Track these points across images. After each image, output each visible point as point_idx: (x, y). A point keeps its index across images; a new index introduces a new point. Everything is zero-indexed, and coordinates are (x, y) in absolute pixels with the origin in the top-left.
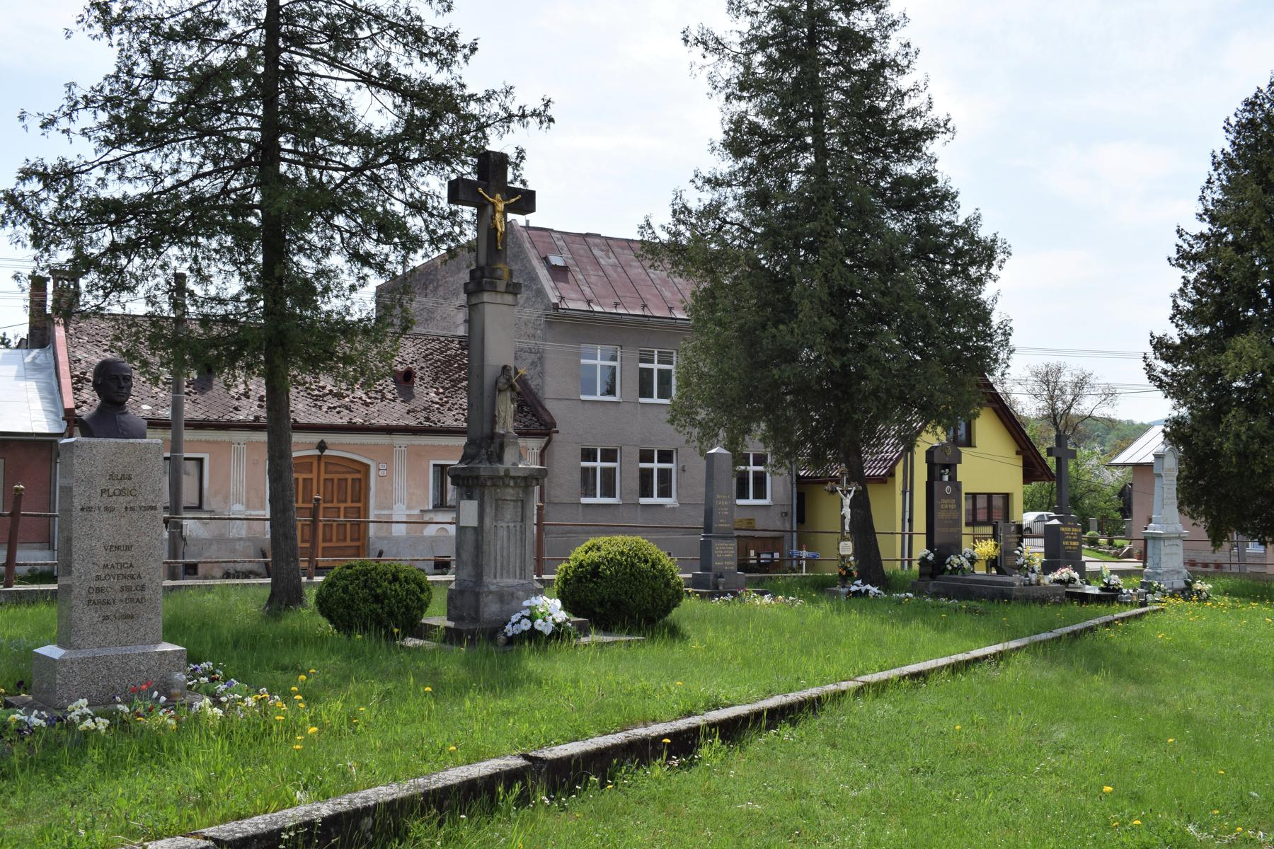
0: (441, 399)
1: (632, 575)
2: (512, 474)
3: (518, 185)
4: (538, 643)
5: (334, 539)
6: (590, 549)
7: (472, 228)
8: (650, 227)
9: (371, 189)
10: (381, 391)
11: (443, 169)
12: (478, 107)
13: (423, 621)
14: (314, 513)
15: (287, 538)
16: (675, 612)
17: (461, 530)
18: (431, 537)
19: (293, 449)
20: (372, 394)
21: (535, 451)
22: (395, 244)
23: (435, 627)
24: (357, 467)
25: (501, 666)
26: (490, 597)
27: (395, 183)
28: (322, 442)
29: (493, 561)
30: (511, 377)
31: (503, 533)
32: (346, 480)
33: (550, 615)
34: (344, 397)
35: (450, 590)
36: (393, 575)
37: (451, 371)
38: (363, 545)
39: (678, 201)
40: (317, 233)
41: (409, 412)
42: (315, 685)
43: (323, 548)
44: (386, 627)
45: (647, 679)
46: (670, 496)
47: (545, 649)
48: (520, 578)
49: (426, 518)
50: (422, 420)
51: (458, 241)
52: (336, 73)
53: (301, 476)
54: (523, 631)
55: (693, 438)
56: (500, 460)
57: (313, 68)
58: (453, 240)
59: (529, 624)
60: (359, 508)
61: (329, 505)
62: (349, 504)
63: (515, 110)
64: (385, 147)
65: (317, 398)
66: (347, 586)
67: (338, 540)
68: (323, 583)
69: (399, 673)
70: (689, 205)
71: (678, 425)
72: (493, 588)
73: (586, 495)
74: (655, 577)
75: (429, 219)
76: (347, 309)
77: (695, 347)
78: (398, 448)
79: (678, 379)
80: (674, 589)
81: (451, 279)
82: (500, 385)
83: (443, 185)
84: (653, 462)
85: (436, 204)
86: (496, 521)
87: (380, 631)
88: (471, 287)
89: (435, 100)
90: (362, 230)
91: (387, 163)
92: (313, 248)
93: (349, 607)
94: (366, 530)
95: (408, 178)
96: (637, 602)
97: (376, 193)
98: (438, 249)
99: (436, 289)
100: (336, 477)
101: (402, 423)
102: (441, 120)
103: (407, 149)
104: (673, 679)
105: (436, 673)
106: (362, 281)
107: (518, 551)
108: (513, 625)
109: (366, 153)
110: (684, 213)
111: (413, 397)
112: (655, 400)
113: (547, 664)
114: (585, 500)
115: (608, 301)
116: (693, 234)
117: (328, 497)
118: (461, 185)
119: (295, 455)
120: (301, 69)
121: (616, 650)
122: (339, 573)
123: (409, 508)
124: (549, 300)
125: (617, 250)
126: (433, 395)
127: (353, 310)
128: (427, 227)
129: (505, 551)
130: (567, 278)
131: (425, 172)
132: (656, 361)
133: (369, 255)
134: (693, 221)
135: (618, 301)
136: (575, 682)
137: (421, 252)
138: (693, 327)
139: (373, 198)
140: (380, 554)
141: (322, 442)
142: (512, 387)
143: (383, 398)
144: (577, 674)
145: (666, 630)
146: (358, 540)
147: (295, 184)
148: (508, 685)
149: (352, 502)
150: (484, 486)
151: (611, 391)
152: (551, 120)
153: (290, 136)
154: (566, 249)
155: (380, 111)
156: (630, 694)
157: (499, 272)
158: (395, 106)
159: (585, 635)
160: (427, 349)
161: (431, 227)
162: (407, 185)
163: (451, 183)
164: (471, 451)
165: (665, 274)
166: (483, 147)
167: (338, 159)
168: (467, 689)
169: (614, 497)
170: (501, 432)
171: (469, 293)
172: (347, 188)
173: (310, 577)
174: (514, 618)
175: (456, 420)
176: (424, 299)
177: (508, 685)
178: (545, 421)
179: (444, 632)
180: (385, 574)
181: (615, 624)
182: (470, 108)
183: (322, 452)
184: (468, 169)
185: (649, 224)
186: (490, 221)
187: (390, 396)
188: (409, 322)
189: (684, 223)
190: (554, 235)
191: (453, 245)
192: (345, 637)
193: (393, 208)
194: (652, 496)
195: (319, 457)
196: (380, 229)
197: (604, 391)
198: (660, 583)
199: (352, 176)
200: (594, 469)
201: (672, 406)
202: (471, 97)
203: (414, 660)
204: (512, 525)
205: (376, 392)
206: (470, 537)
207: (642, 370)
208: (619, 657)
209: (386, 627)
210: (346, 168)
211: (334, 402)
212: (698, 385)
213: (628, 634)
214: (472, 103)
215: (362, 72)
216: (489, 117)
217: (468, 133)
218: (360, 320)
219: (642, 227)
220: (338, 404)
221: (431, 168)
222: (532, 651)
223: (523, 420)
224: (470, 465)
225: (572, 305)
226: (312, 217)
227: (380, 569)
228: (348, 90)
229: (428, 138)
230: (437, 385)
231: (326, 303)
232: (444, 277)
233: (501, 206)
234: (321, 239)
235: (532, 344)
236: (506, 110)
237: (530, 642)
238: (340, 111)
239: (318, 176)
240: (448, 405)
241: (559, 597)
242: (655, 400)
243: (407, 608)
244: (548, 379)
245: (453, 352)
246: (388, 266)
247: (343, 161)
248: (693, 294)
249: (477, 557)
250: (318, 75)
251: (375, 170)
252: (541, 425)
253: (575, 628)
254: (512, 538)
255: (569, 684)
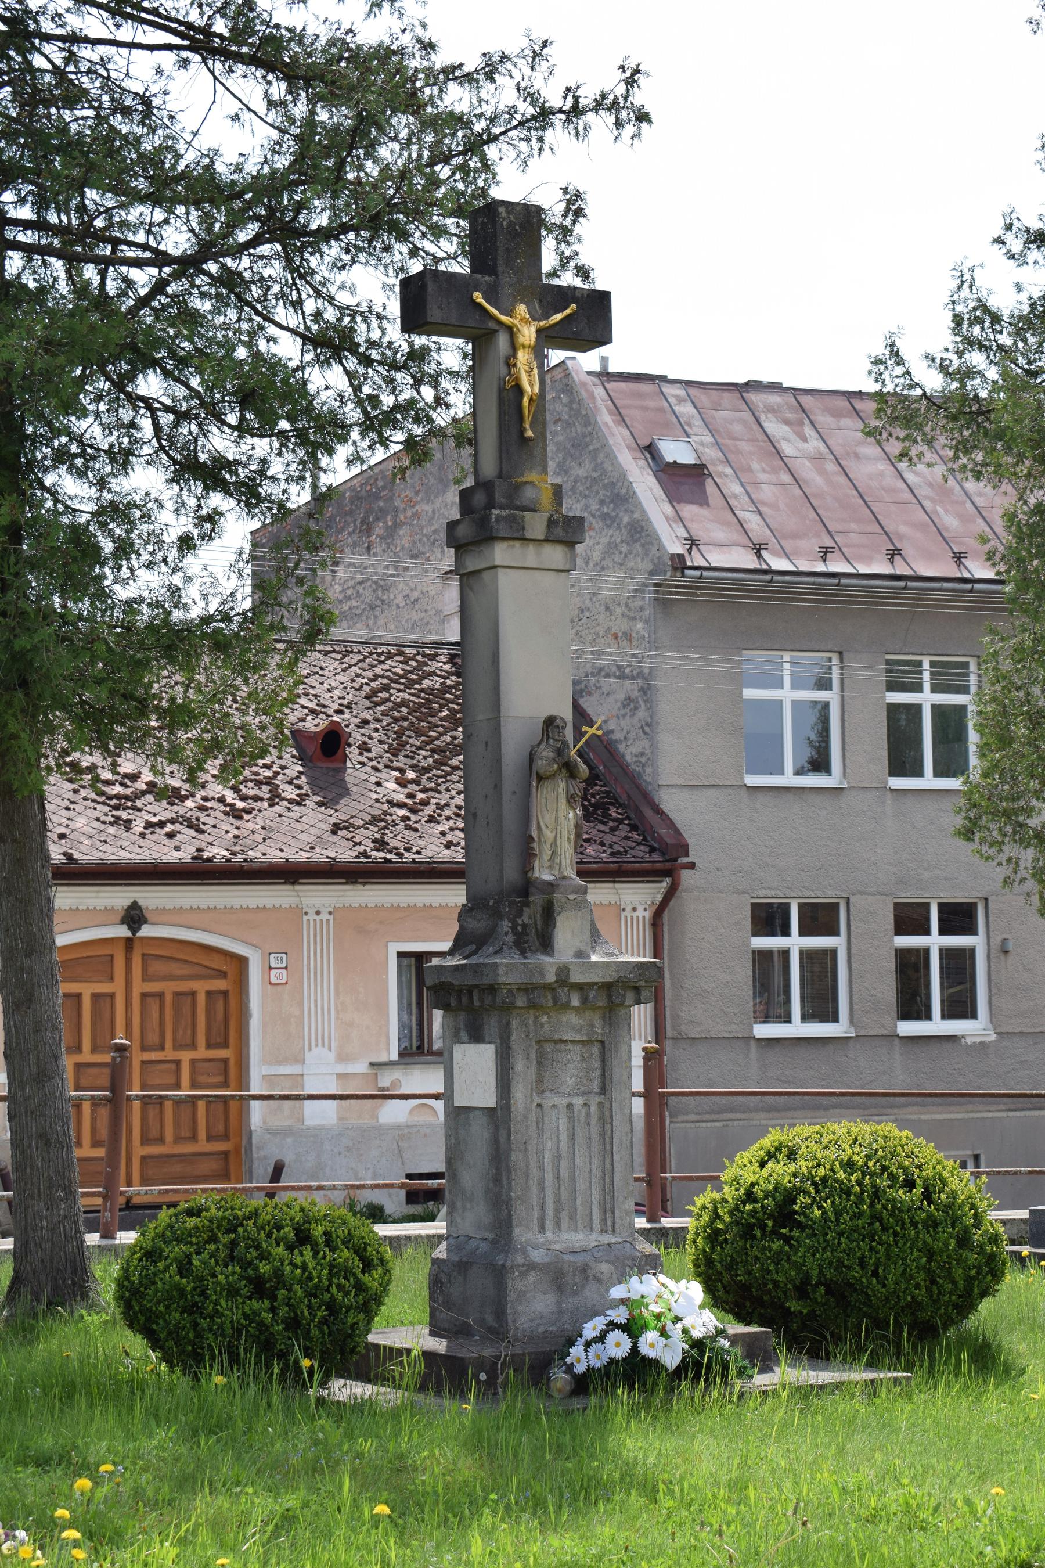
0: (411, 796)
1: (876, 1217)
2: (576, 977)
3: (568, 279)
4: (648, 1391)
5: (169, 1136)
6: (771, 1155)
7: (463, 386)
8: (899, 362)
9: (221, 303)
10: (268, 782)
11: (387, 249)
12: (466, 96)
13: (371, 1338)
14: (117, 1080)
15: (47, 1143)
16: (985, 1306)
17: (457, 1115)
18: (398, 1127)
19: (56, 929)
20: (250, 790)
21: (640, 913)
22: (282, 434)
23: (400, 1352)
24: (217, 963)
25: (559, 1449)
26: (532, 1278)
27: (276, 288)
28: (135, 906)
29: (535, 1189)
30: (565, 743)
31: (557, 1123)
32: (193, 994)
33: (677, 1319)
34: (183, 799)
35: (435, 1261)
36: (298, 1230)
37: (433, 727)
38: (237, 1150)
39: (965, 292)
40: (97, 415)
41: (336, 829)
42: (114, 1501)
43: (144, 1158)
44: (283, 1355)
45: (918, 1480)
46: (974, 1016)
47: (667, 1402)
48: (604, 1231)
49: (386, 1079)
50: (368, 846)
51: (430, 420)
52: (127, 32)
53: (87, 990)
54: (612, 1361)
55: (1022, 873)
56: (546, 944)
57: (75, 22)
58: (417, 420)
59: (627, 1344)
60: (225, 1061)
61: (153, 1056)
62: (202, 1052)
63: (554, 98)
64: (249, 205)
65: (120, 802)
66: (188, 1257)
67: (178, 1139)
68: (132, 1249)
69: (314, 1469)
70: (993, 303)
71: (983, 841)
72: (537, 1256)
73: (766, 1018)
74: (932, 1224)
75: (361, 370)
76: (174, 592)
77: (1019, 649)
78: (312, 916)
79: (980, 728)
80: (981, 1251)
81: (428, 508)
82: (540, 764)
83: (391, 288)
84: (927, 932)
85: (375, 335)
86: (541, 1093)
87: (269, 1367)
88: (462, 531)
89: (363, 85)
90: (203, 404)
91: (256, 241)
92: (88, 451)
93: (192, 1309)
94: (244, 1114)
95: (304, 274)
96: (890, 1283)
97: (232, 314)
98: (384, 442)
99: (391, 532)
100: (169, 988)
101: (321, 855)
102: (381, 130)
103: (299, 207)
104: (982, 1478)
105: (401, 1466)
106: (208, 526)
107: (596, 1164)
108: (588, 1345)
109: (207, 219)
110: (979, 321)
111: (346, 792)
112: (929, 781)
113: (671, 1443)
114: (764, 1031)
115: (803, 544)
116: (1005, 374)
117: (153, 1038)
118: (431, 287)
119: (61, 941)
120: (47, 26)
121: (840, 1404)
122: (170, 1227)
123: (342, 1058)
124: (661, 548)
125: (823, 419)
126: (392, 785)
127: (192, 593)
128: (357, 389)
129: (564, 1164)
130: (704, 492)
131: (347, 258)
132: (927, 686)
133: (221, 463)
134: (1005, 340)
135: (828, 543)
136: (738, 1487)
137: (343, 451)
138: (1014, 600)
139: (225, 327)
140: (277, 1172)
141: (135, 906)
142: (569, 769)
143: (275, 798)
144: (744, 1466)
145: (964, 1355)
146: (226, 1137)
147: (42, 303)
148: (575, 1497)
149: (209, 1046)
150: (508, 1008)
151: (819, 764)
152: (643, 117)
153: (26, 188)
154: (698, 422)
155: (235, 118)
156: (874, 1518)
157: (529, 493)
158: (271, 104)
159: (766, 1369)
160: (376, 677)
161: (367, 390)
162: (306, 291)
163: (405, 284)
164: (478, 924)
165: (940, 470)
166: (484, 192)
167: (141, 237)
168: (476, 1506)
169: (836, 1020)
170: (547, 877)
171: (460, 547)
172: (164, 308)
173: (108, 1234)
174: (591, 1329)
175: (448, 845)
176: (366, 559)
177: (575, 1497)
178: (660, 839)
179: (421, 1367)
180: (279, 1227)
181: (838, 1339)
182: (447, 100)
183: (134, 932)
184: (448, 246)
185: (895, 353)
186: (504, 370)
187: (290, 793)
188: (322, 618)
189: (982, 347)
190: (667, 389)
191: (418, 431)
192: (188, 1381)
193: (274, 349)
194: (929, 1017)
195: (129, 943)
196: (245, 399)
197: (804, 761)
198: (946, 1239)
199: (176, 276)
200: (785, 953)
201: (968, 794)
202: (449, 71)
203: (349, 1435)
204: (578, 1101)
205: (259, 783)
206: (479, 1132)
207: (893, 709)
208: (850, 1421)
209: (283, 1355)
210: (161, 259)
211: (161, 811)
212: (1031, 742)
213: (870, 1365)
214: (452, 86)
215: (189, 26)
216: (492, 120)
217: (446, 160)
218: (206, 620)
219: (878, 362)
220: (168, 815)
221: (359, 249)
222: (633, 1412)
223: (609, 839)
224: (475, 960)
225: (717, 558)
226: (83, 380)
227: (264, 1217)
228: (159, 72)
229: (350, 176)
230: (401, 761)
231: (125, 583)
232: (411, 503)
233: (528, 334)
234: (107, 429)
235: (623, 655)
236: (532, 97)
237: (631, 1389)
238: (142, 123)
239: (96, 280)
240: (429, 810)
241: (698, 1275)
242: (929, 781)
243: (332, 1307)
244: (665, 739)
245: (436, 682)
246: (267, 489)
247: (152, 243)
248: (1010, 517)
249: (497, 1180)
250: (86, 40)
251: (228, 261)
252: (652, 850)
253: (738, 1350)
254: (580, 1140)
255: (723, 1493)
